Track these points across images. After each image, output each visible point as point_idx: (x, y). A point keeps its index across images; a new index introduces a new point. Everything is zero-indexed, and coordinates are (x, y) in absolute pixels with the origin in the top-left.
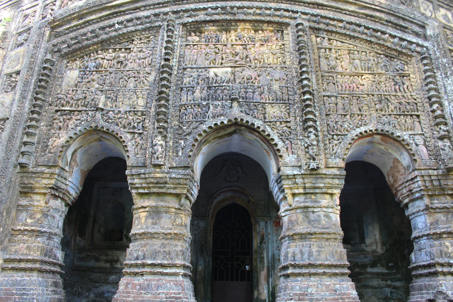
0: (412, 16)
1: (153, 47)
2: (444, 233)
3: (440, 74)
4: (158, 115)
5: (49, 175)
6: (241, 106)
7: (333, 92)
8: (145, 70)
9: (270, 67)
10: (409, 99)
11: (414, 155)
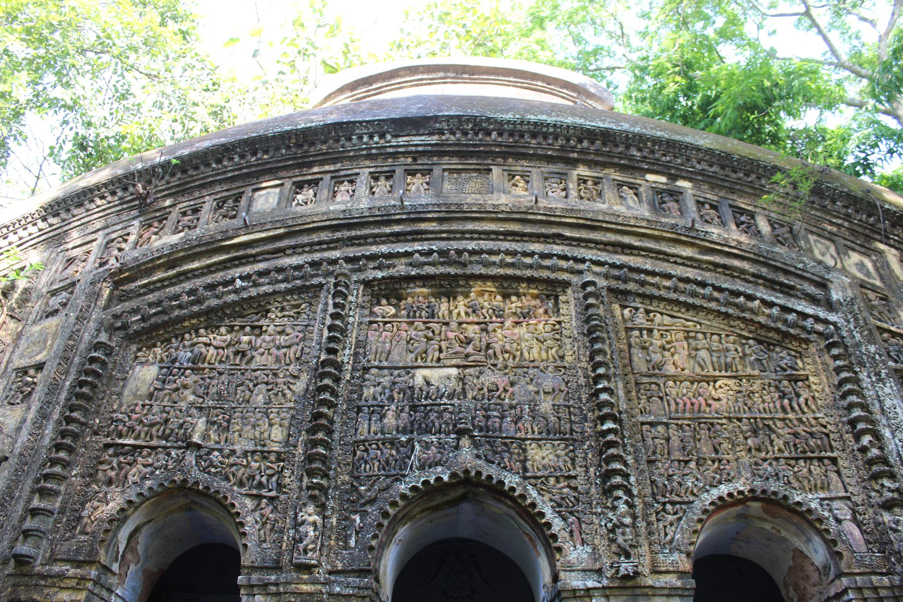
0: (800, 266)
3: (866, 374)
4: (311, 462)
5: (76, 581)
6: (476, 445)
7: (659, 415)
8: (287, 370)
9: (534, 367)
10: (812, 426)
11: (834, 542)
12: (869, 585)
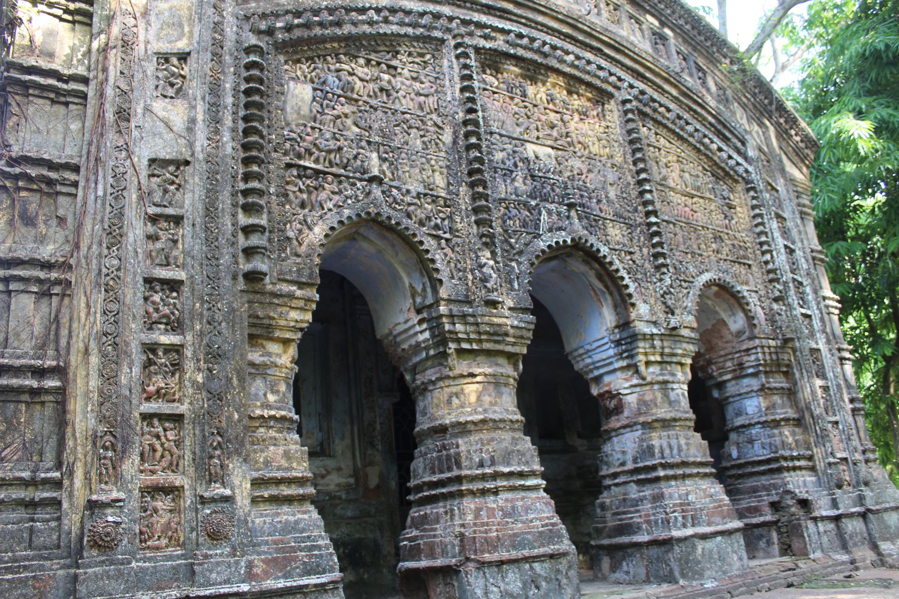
1: (436, 78)
2: (782, 419)
11: (753, 318)
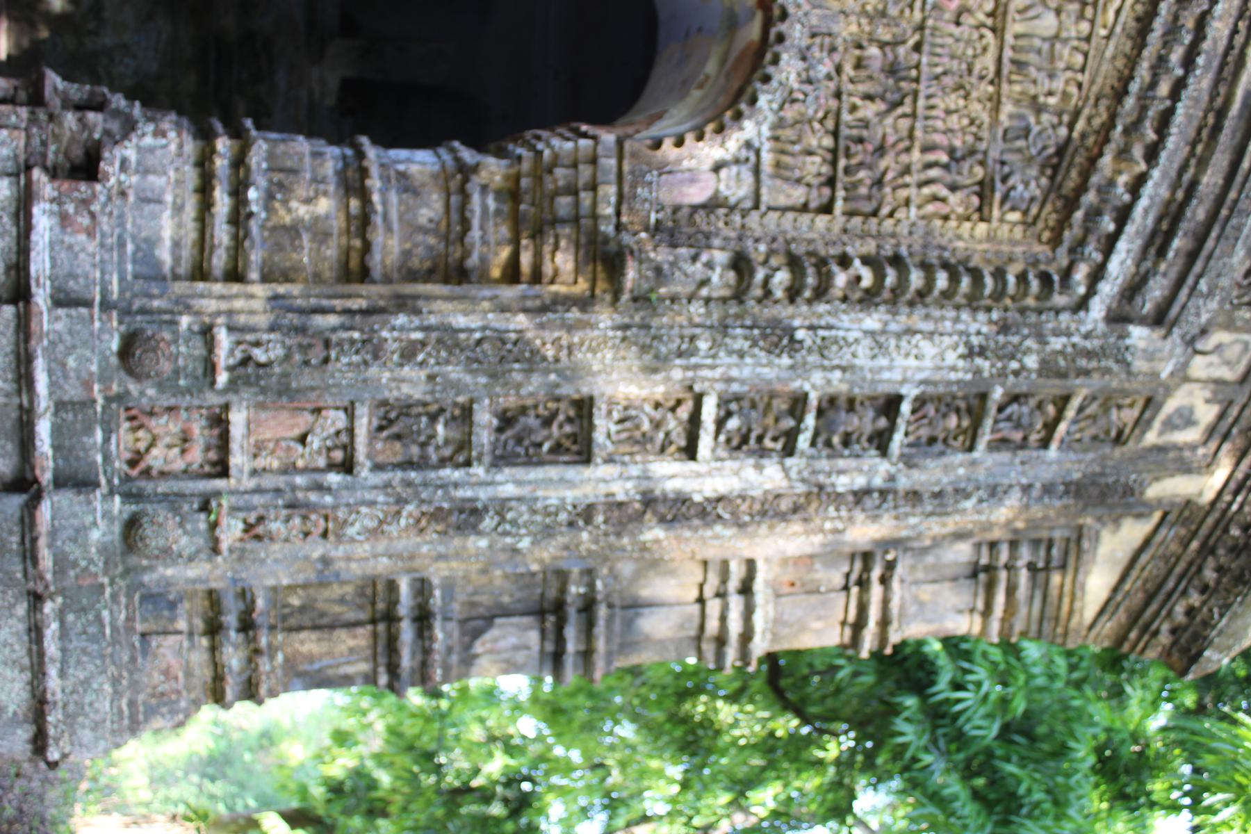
0: (1203, 285)
10: (894, 189)
12: (600, 178)
